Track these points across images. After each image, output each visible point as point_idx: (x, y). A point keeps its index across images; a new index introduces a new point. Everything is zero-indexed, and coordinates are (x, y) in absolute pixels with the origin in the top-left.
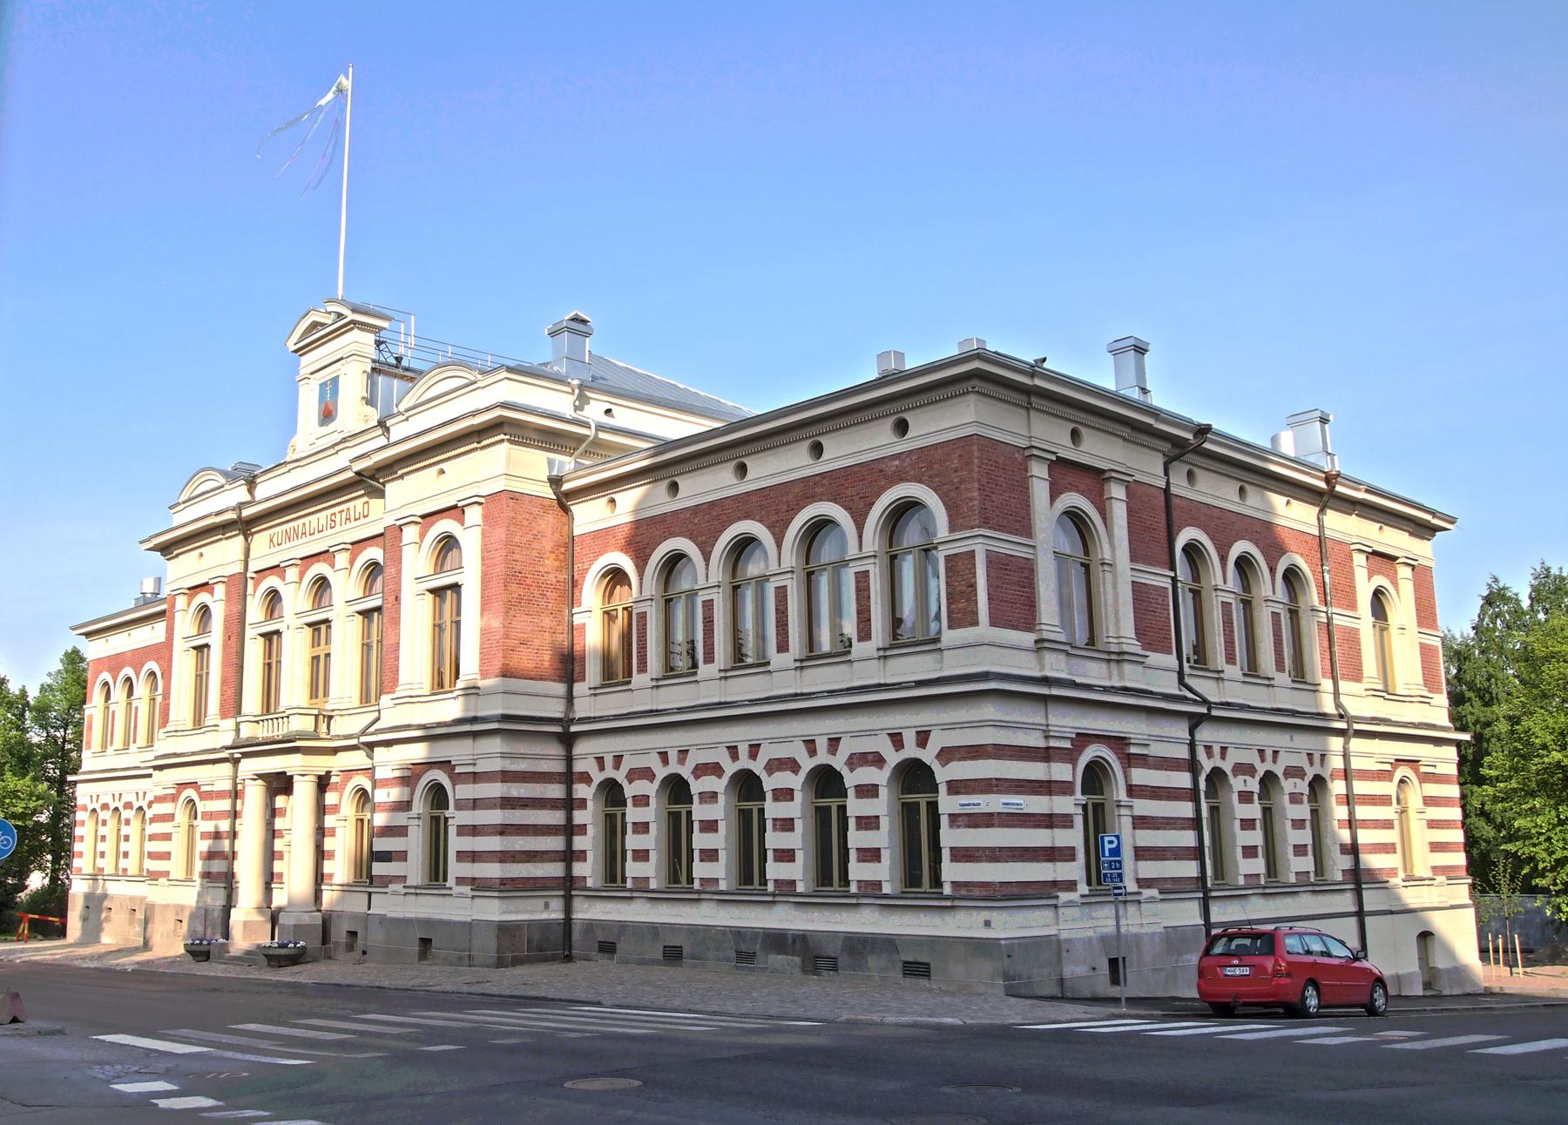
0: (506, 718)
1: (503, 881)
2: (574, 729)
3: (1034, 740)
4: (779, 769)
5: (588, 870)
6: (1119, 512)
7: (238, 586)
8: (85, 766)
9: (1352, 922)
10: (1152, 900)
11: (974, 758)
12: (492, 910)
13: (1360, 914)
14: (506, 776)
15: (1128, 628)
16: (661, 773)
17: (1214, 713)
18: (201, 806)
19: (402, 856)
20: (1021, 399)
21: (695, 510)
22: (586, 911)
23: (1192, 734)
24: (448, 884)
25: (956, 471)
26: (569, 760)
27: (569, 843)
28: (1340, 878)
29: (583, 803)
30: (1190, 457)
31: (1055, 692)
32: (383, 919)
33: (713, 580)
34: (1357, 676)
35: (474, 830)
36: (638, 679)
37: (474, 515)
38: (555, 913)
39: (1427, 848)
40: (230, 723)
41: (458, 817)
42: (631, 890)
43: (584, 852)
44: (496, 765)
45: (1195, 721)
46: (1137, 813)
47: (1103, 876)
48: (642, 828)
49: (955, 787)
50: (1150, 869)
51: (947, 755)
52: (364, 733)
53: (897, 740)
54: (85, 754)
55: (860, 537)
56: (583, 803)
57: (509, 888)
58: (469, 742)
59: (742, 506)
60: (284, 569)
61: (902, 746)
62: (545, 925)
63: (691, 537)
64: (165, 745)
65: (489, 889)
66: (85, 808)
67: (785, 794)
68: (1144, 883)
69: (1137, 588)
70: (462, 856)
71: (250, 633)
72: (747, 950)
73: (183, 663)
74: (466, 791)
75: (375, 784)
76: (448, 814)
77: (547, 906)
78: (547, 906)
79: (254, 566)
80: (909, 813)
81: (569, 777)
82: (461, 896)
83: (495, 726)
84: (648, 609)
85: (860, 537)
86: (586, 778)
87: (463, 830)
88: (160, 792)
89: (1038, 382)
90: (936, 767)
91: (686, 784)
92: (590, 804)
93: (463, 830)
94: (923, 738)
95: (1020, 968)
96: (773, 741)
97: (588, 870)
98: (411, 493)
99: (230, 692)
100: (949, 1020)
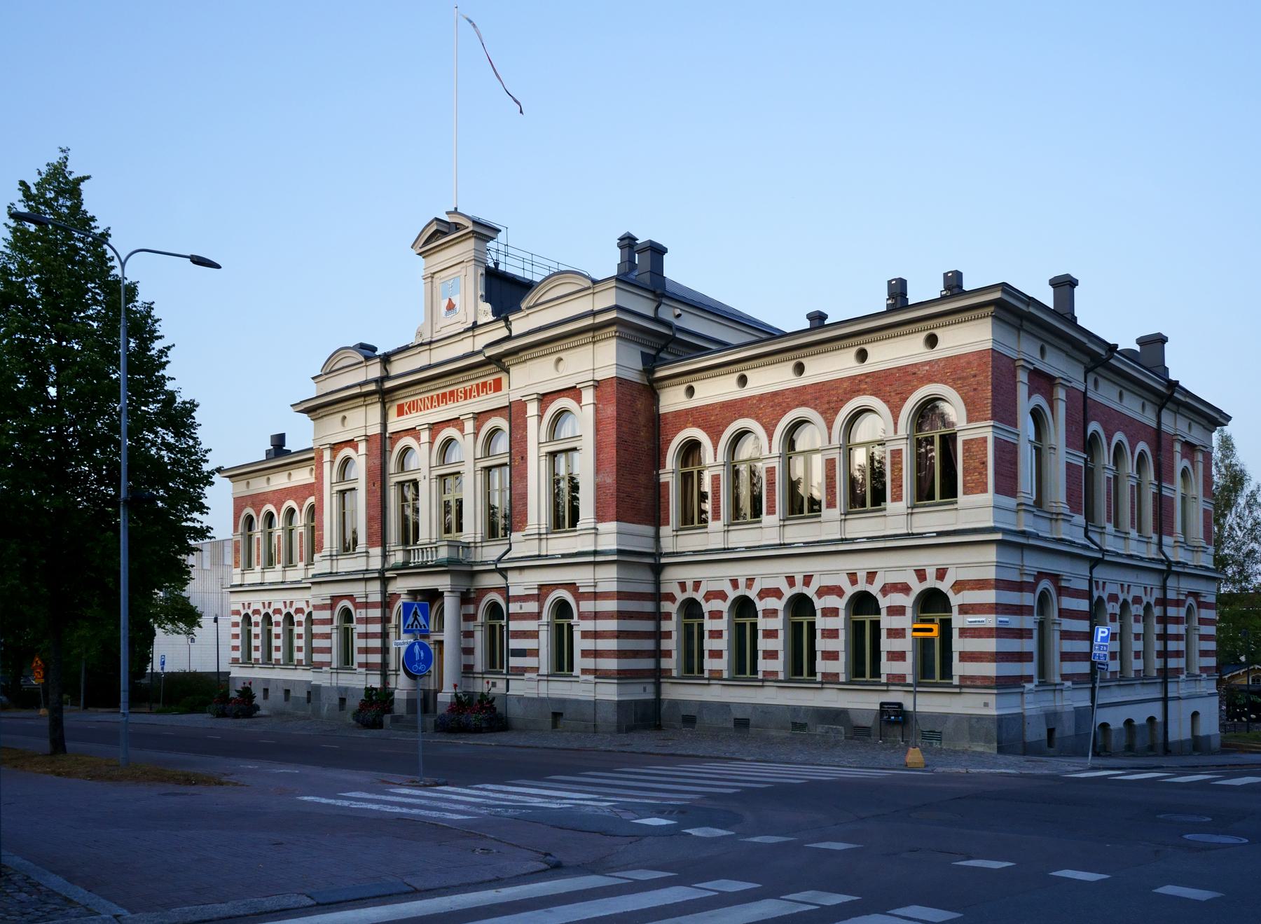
2: (663, 561)
4: (715, 598)
5: (672, 664)
6: (1061, 408)
9: (1159, 705)
10: (1068, 689)
11: (980, 589)
12: (609, 692)
13: (1165, 700)
17: (1107, 558)
18: (358, 614)
20: (1016, 321)
21: (762, 397)
22: (675, 692)
25: (975, 376)
26: (657, 583)
27: (658, 644)
28: (1155, 674)
29: (668, 616)
30: (1100, 370)
31: (1031, 542)
32: (520, 698)
34: (1171, 534)
37: (362, 447)
38: (649, 695)
43: (670, 651)
45: (1094, 563)
47: (347, 660)
48: (771, 634)
49: (965, 609)
51: (959, 586)
52: (499, 560)
53: (921, 575)
55: (896, 424)
56: (668, 616)
58: (591, 568)
59: (800, 396)
61: (925, 579)
62: (645, 702)
64: (321, 566)
67: (716, 615)
68: (1065, 677)
69: (1069, 465)
72: (800, 724)
74: (587, 606)
75: (508, 600)
77: (645, 689)
78: (645, 689)
80: (796, 629)
81: (658, 596)
85: (896, 424)
86: (671, 597)
87: (585, 635)
88: (320, 602)
89: (1032, 310)
90: (951, 594)
91: (752, 603)
92: (674, 617)
93: (585, 635)
94: (941, 573)
96: (823, 573)
97: (672, 664)
98: (526, 379)
100: (955, 770)
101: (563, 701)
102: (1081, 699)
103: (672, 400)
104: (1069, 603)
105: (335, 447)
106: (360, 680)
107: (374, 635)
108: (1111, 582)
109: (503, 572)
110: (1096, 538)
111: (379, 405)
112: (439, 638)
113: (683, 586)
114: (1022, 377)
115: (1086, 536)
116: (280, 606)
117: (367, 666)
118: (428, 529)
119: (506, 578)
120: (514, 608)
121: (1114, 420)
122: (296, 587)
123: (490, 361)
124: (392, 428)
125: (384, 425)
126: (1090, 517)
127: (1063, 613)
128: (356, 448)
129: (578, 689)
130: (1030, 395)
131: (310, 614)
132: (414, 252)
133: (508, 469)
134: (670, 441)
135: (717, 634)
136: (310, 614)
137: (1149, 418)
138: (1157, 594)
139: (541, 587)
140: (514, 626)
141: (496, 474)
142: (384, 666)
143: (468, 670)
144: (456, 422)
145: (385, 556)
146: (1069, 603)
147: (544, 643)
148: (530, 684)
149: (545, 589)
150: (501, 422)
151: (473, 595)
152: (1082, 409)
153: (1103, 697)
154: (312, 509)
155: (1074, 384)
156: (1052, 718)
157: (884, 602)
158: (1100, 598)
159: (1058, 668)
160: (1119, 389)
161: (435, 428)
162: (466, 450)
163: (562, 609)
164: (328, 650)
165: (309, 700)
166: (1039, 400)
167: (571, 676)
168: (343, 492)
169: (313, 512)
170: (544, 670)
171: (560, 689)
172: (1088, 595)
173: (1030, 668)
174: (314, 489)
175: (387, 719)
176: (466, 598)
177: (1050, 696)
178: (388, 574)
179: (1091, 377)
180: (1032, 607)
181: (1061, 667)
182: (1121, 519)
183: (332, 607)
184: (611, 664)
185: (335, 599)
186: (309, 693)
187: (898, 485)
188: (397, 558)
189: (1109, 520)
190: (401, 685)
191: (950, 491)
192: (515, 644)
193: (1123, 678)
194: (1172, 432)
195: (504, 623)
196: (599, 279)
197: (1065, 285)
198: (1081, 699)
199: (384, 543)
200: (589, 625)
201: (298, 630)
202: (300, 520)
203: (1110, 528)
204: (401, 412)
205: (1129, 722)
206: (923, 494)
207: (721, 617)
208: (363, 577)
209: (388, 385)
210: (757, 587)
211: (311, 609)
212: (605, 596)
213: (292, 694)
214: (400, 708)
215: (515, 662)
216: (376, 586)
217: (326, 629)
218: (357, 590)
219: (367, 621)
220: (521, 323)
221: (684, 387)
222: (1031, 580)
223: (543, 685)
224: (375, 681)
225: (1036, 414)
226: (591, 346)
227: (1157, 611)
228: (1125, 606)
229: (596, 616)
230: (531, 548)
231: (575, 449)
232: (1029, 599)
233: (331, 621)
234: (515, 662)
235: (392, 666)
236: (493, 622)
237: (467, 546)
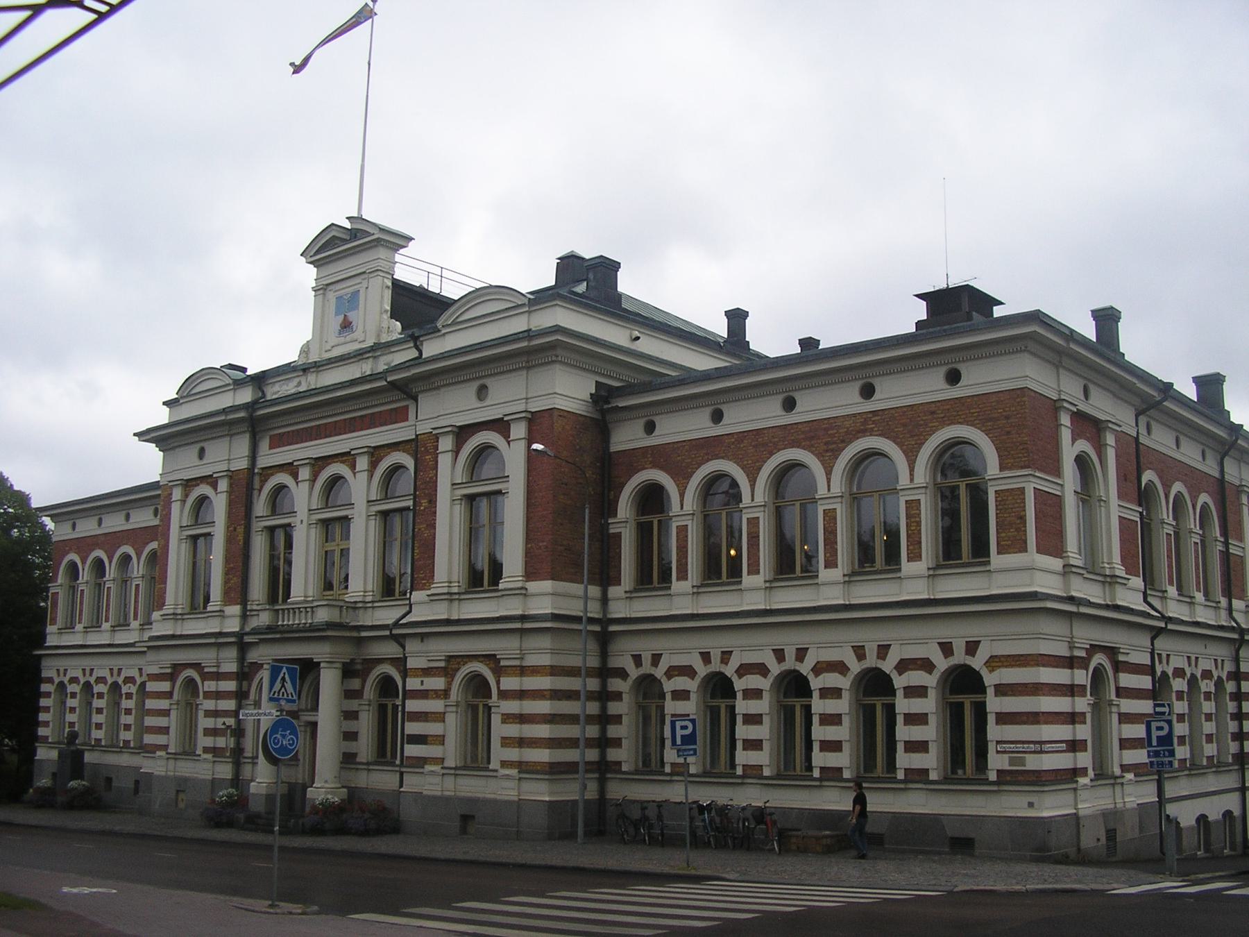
0: (555, 617)
1: (552, 765)
2: (613, 628)
3: (1062, 650)
5: (624, 755)
6: (1111, 454)
8: (51, 641)
9: (1236, 796)
12: (540, 792)
14: (554, 671)
15: (1117, 558)
17: (1170, 627)
19: (440, 740)
22: (617, 791)
23: (1152, 644)
24: (491, 767)
26: (604, 655)
29: (618, 696)
37: (223, 485)
40: (236, 609)
44: (545, 660)
45: (1156, 633)
46: (1123, 710)
51: (995, 662)
52: (397, 624)
54: (50, 629)
64: (161, 628)
65: (537, 772)
66: (50, 680)
68: (1125, 768)
70: (506, 742)
71: (257, 526)
74: (211, 686)
75: (405, 673)
81: (605, 672)
83: (548, 625)
86: (622, 674)
90: (984, 673)
93: (507, 718)
95: (1036, 842)
98: (442, 410)
99: (236, 580)
101: (473, 801)
102: (1145, 793)
103: (628, 437)
104: (1127, 680)
105: (189, 484)
107: (225, 713)
108: (1176, 655)
109: (400, 640)
110: (1156, 603)
111: (247, 435)
112: (312, 719)
113: (637, 660)
114: (1065, 420)
115: (1145, 601)
116: (105, 673)
117: (214, 751)
118: (303, 584)
119: (403, 647)
120: (413, 683)
121: (1170, 469)
122: (127, 651)
123: (393, 385)
124: (263, 462)
125: (253, 457)
126: (1149, 580)
127: (1121, 692)
128: (214, 485)
129: (502, 788)
130: (1074, 441)
131: (143, 684)
132: (303, 259)
133: (411, 514)
134: (622, 485)
135: (831, 720)
136: (143, 684)
137: (1210, 467)
138: (1229, 667)
139: (449, 658)
140: (413, 705)
141: (397, 520)
142: (238, 752)
143: (348, 759)
144: (347, 458)
145: (244, 616)
146: (1127, 680)
147: (452, 728)
148: (433, 777)
151: (359, 667)
152: (1135, 458)
153: (1171, 790)
154: (153, 556)
155: (1124, 429)
156: (1111, 818)
157: (899, 682)
158: (1164, 673)
159: (1120, 757)
160: (1174, 434)
161: (319, 463)
162: (361, 488)
163: (478, 686)
164: (165, 730)
165: (136, 791)
166: (1083, 445)
167: (487, 769)
168: (195, 538)
169: (157, 561)
170: (450, 762)
171: (471, 787)
172: (1150, 670)
173: (1084, 759)
174: (159, 532)
176: (348, 671)
177: (1108, 791)
178: (247, 639)
179: (1143, 420)
180: (1085, 686)
181: (1121, 756)
182: (1211, 589)
183: (172, 677)
184: (542, 755)
185: (177, 668)
186: (137, 782)
187: (915, 541)
188: (264, 619)
189: (1171, 583)
190: (262, 778)
191: (980, 550)
192: (412, 728)
193: (1194, 766)
194: (1238, 483)
195: (399, 702)
197: (1107, 319)
198: (1145, 793)
199: (244, 601)
200: (512, 706)
201: (126, 704)
202: (138, 569)
203: (1172, 591)
205: (1202, 819)
206: (949, 552)
207: (688, 698)
208: (217, 641)
210: (734, 663)
211: (144, 678)
212: (535, 671)
213: (114, 784)
215: (412, 750)
216: (233, 653)
217: (164, 704)
218: (206, 657)
219: (218, 695)
220: (431, 348)
221: (642, 422)
222: (1083, 654)
223: (449, 782)
225: (1082, 462)
226: (524, 372)
227: (1230, 687)
228: (1193, 682)
229: (522, 695)
230: (440, 612)
231: (499, 492)
232: (1082, 677)
233: (169, 695)
234: (412, 750)
235: (248, 753)
236: (384, 701)
237: (354, 607)
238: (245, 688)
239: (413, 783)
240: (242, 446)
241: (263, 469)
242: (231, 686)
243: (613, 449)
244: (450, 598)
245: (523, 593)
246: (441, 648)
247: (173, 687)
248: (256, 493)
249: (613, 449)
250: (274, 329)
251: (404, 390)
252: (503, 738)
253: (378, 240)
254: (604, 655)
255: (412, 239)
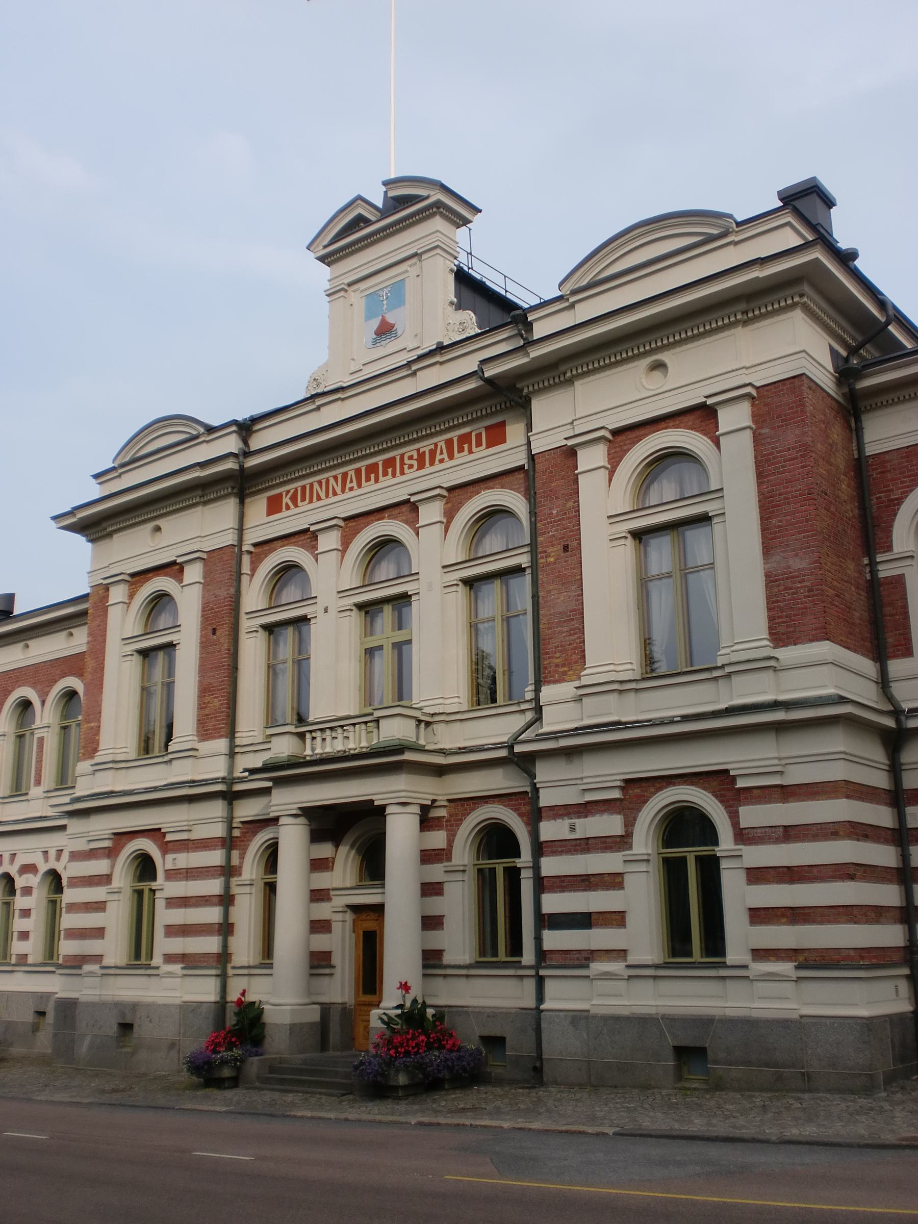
7: (226, 566)
16: (43, 868)
18: (163, 862)
19: (617, 919)
24: (154, 963)
33: (45, 722)
35: (184, 902)
36: (35, 792)
37: (194, 573)
39: (746, 918)
40: (221, 745)
41: (167, 888)
42: (14, 965)
50: (178, 945)
52: (515, 740)
57: (815, 962)
60: (314, 536)
63: (34, 686)
64: (89, 782)
71: (246, 624)
73: (121, 678)
76: (154, 885)
79: (252, 537)
82: (170, 975)
84: (45, 735)
98: (554, 418)
99: (217, 703)
101: (705, 1023)
106: (175, 991)
119: (533, 776)
120: (550, 830)
129: (755, 993)
132: (311, 256)
143: (432, 959)
144: (407, 508)
149: (638, 789)
150: (512, 499)
151: (442, 813)
162: (434, 549)
167: (148, 967)
171: (691, 997)
175: (254, 1065)
196: (216, 423)
204: (274, 506)
209: (252, 462)
214: (278, 1044)
224: (204, 990)
231: (704, 519)
238: (235, 861)
239: (563, 996)
240: (227, 510)
241: (255, 545)
242: (215, 858)
243: (870, 450)
244: (621, 688)
245: (769, 665)
246: (606, 773)
247: (113, 866)
248: (245, 579)
249: (870, 450)
250: (276, 344)
251: (503, 398)
252: (750, 909)
253: (438, 204)
254: (895, 770)
255: (480, 211)
